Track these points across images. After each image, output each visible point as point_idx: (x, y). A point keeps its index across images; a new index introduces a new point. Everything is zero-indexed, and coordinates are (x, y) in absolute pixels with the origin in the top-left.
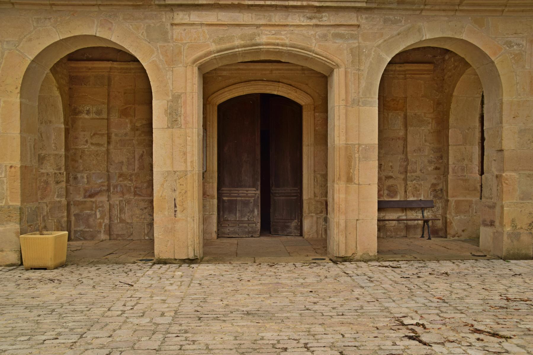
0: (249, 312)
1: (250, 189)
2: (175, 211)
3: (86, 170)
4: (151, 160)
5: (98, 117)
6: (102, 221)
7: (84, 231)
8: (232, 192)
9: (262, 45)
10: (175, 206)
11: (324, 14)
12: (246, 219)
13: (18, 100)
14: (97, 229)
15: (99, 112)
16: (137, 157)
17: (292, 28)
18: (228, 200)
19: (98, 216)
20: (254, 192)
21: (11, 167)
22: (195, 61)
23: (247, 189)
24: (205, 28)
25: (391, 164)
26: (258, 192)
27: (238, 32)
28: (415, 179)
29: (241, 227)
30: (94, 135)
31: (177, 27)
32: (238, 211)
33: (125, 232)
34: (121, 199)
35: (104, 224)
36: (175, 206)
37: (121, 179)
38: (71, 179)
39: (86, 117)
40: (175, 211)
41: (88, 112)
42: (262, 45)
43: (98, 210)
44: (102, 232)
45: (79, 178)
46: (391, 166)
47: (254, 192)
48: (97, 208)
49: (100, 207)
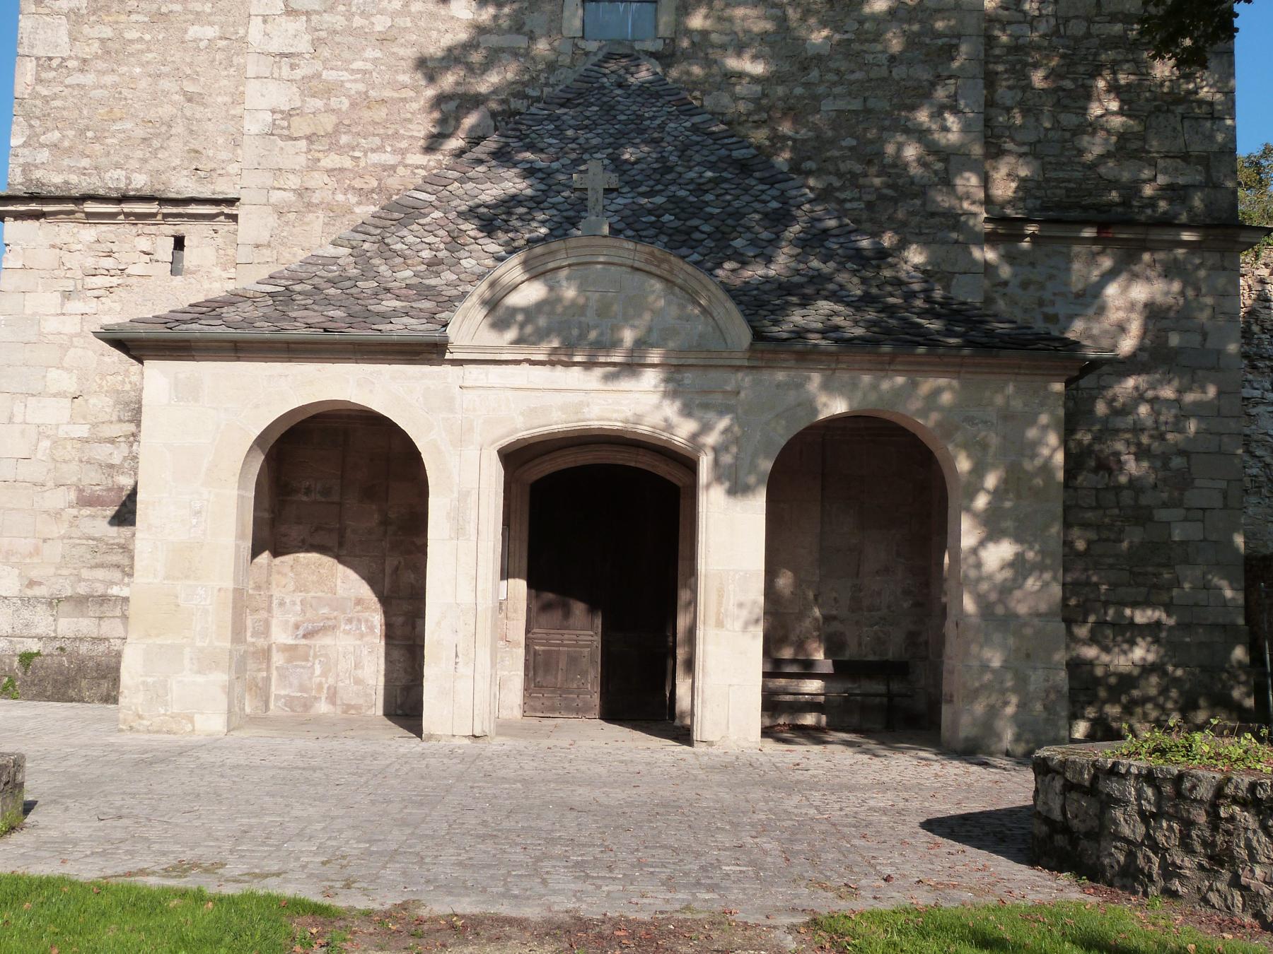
0: (392, 172)
1: (582, 632)
2: (456, 663)
3: (301, 591)
4: (411, 577)
5: (323, 500)
6: (323, 680)
7: (290, 697)
8: (551, 636)
9: (593, 420)
10: (457, 656)
11: (686, 375)
12: (575, 686)
13: (235, 492)
14: (314, 693)
15: (326, 492)
16: (388, 570)
17: (637, 395)
18: (543, 651)
19: (318, 671)
20: (590, 638)
21: (220, 590)
22: (493, 443)
23: (579, 632)
24: (510, 393)
25: (834, 594)
26: (598, 639)
27: (559, 399)
28: (877, 624)
29: (566, 699)
30: (316, 530)
31: (470, 391)
32: (560, 672)
33: (361, 701)
34: (358, 642)
35: (326, 686)
36: (457, 656)
37: (359, 608)
38: (274, 605)
39: (305, 498)
40: (456, 663)
41: (308, 491)
42: (593, 420)
43: (317, 662)
44: (324, 697)
45: (288, 604)
46: (835, 599)
47: (590, 638)
48: (315, 656)
49: (321, 655)
